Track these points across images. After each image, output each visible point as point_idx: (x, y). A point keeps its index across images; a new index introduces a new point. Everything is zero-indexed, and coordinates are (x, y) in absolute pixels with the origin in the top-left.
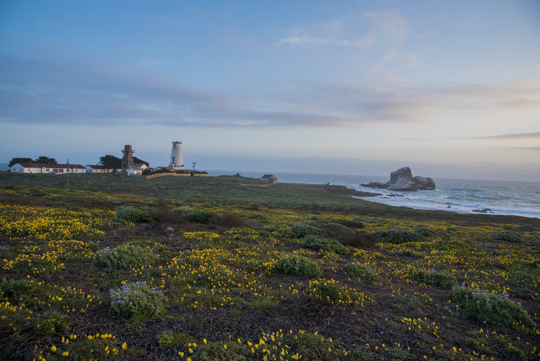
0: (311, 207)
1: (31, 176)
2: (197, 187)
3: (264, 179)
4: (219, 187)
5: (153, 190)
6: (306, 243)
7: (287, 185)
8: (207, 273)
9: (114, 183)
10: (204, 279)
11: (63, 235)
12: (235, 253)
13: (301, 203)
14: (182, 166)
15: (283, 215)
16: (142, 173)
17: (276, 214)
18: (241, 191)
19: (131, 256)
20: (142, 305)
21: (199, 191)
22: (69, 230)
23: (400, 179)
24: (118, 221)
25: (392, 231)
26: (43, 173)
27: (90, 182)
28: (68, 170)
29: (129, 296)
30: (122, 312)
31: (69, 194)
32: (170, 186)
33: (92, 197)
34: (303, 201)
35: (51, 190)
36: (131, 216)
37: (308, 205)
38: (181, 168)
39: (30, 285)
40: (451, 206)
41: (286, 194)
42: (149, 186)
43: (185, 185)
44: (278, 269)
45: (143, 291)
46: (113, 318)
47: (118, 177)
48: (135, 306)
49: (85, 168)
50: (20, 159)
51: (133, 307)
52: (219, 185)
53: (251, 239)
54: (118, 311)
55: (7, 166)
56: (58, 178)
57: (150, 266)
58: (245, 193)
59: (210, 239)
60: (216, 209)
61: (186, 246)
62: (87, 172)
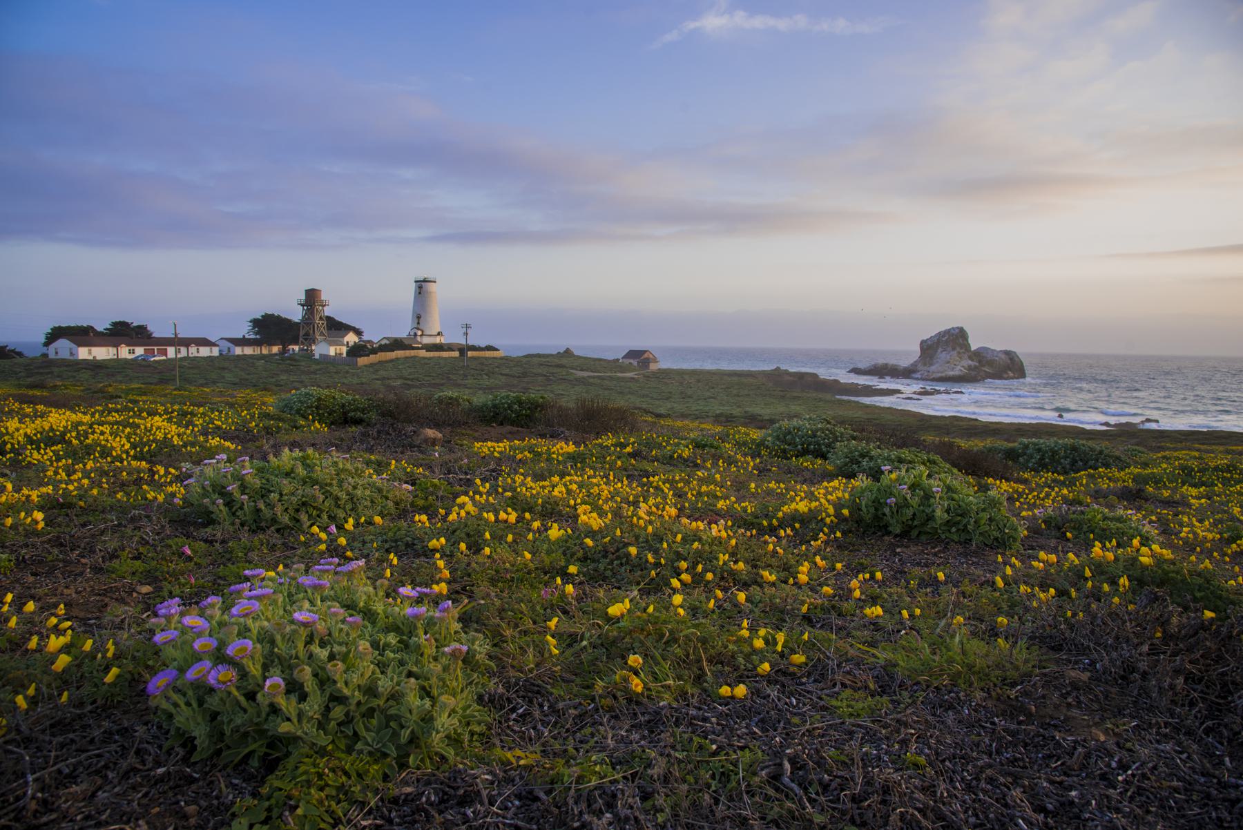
3: (627, 361)
4: (526, 380)
6: (846, 464)
7: (681, 373)
8: (618, 532)
9: (284, 377)
13: (718, 412)
14: (439, 334)
16: (348, 353)
18: (577, 388)
19: (305, 483)
20: (346, 692)
21: (480, 389)
23: (942, 356)
25: (1035, 444)
29: (266, 639)
35: (133, 389)
36: (317, 408)
38: (437, 340)
40: (1065, 415)
41: (682, 393)
42: (364, 380)
44: (859, 522)
45: (350, 606)
46: (161, 779)
48: (303, 697)
49: (217, 346)
50: (69, 328)
51: (287, 705)
52: (524, 375)
53: (676, 456)
54: (200, 732)
56: (156, 368)
57: (378, 519)
59: (555, 456)
62: (221, 354)
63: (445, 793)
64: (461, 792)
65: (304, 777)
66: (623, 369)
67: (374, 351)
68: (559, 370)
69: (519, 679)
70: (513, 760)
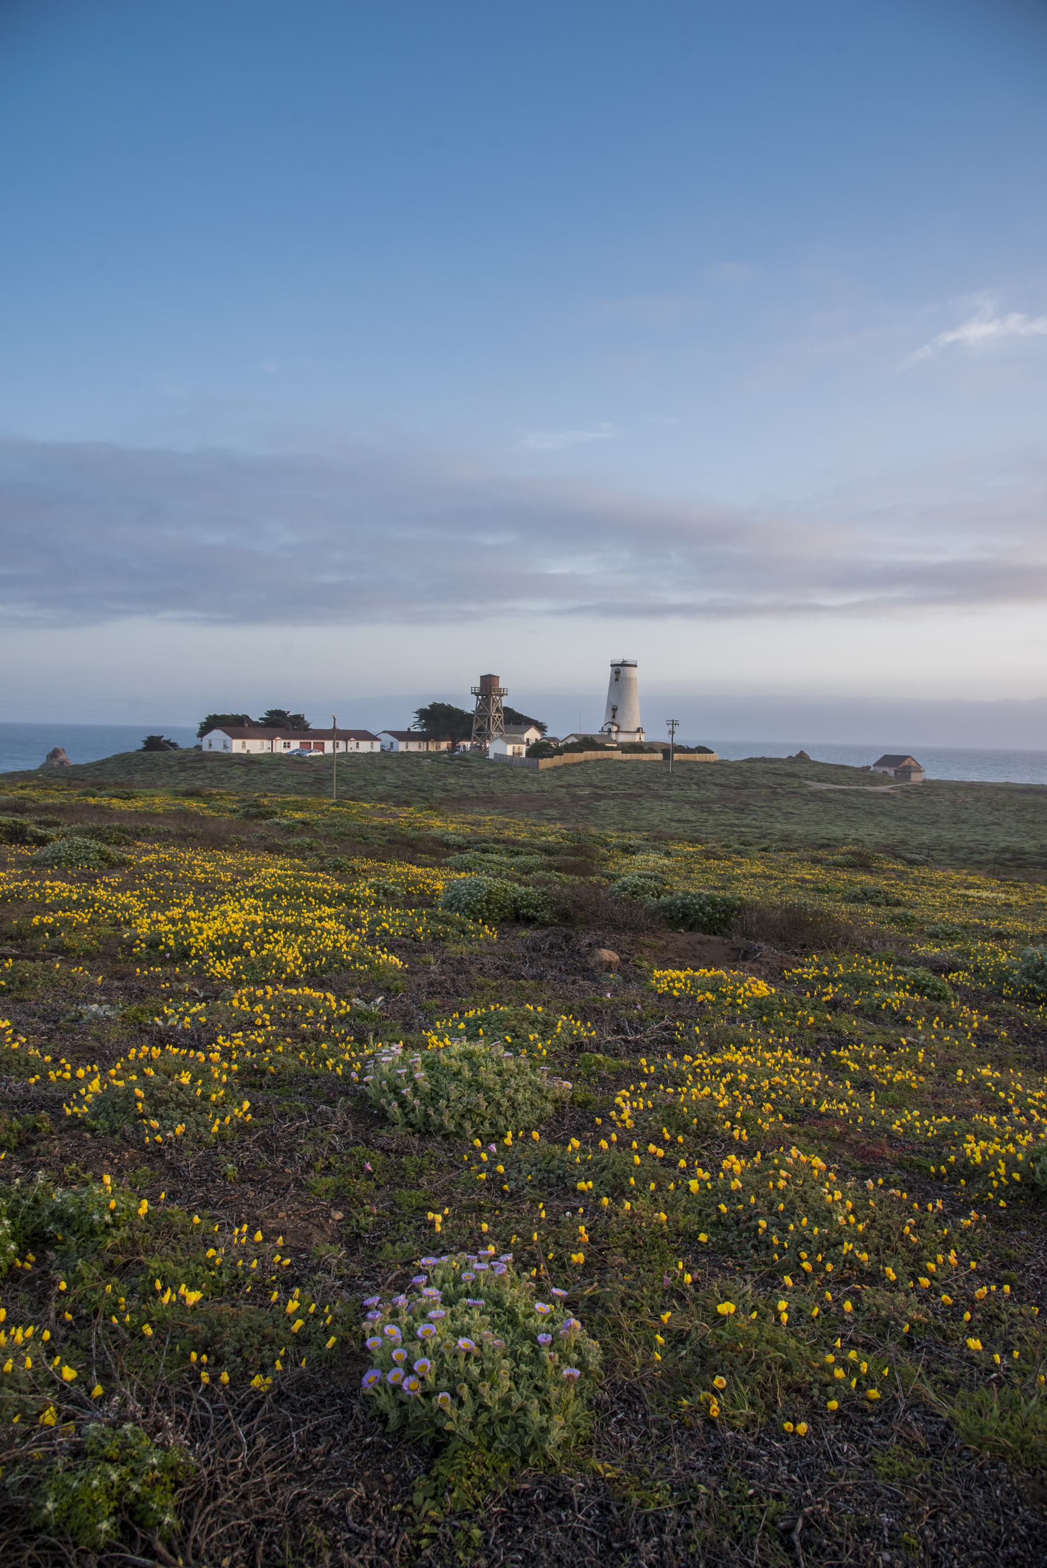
0: (1036, 858)
1: (249, 761)
2: (681, 792)
3: (880, 770)
4: (745, 792)
5: (557, 800)
10: (741, 1226)
11: (281, 968)
12: (835, 1069)
13: (1003, 845)
14: (638, 730)
15: (954, 887)
16: (529, 753)
17: (931, 885)
18: (811, 805)
19: (470, 1086)
20: (490, 1404)
21: (686, 803)
22: (300, 948)
24: (447, 922)
26: (275, 754)
27: (390, 778)
28: (335, 746)
30: (406, 1417)
31: (333, 812)
32: (603, 788)
33: (392, 821)
34: (1007, 839)
35: (288, 803)
36: (487, 902)
37: (1028, 853)
38: (636, 738)
39: (108, 1218)
41: (953, 816)
42: (546, 787)
43: (648, 787)
46: (368, 1446)
47: (464, 763)
49: (379, 740)
50: (224, 717)
52: (744, 785)
53: (883, 1006)
55: (195, 736)
56: (311, 765)
58: (824, 811)
59: (740, 1001)
60: (740, 864)
61: (660, 1028)
62: (382, 750)
63: (550, 1493)
64: (561, 1495)
65: (458, 1467)
66: (874, 780)
67: (559, 752)
68: (789, 780)
69: (624, 1382)
70: (602, 1471)
